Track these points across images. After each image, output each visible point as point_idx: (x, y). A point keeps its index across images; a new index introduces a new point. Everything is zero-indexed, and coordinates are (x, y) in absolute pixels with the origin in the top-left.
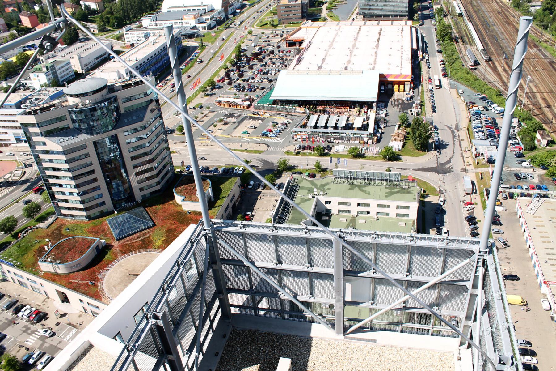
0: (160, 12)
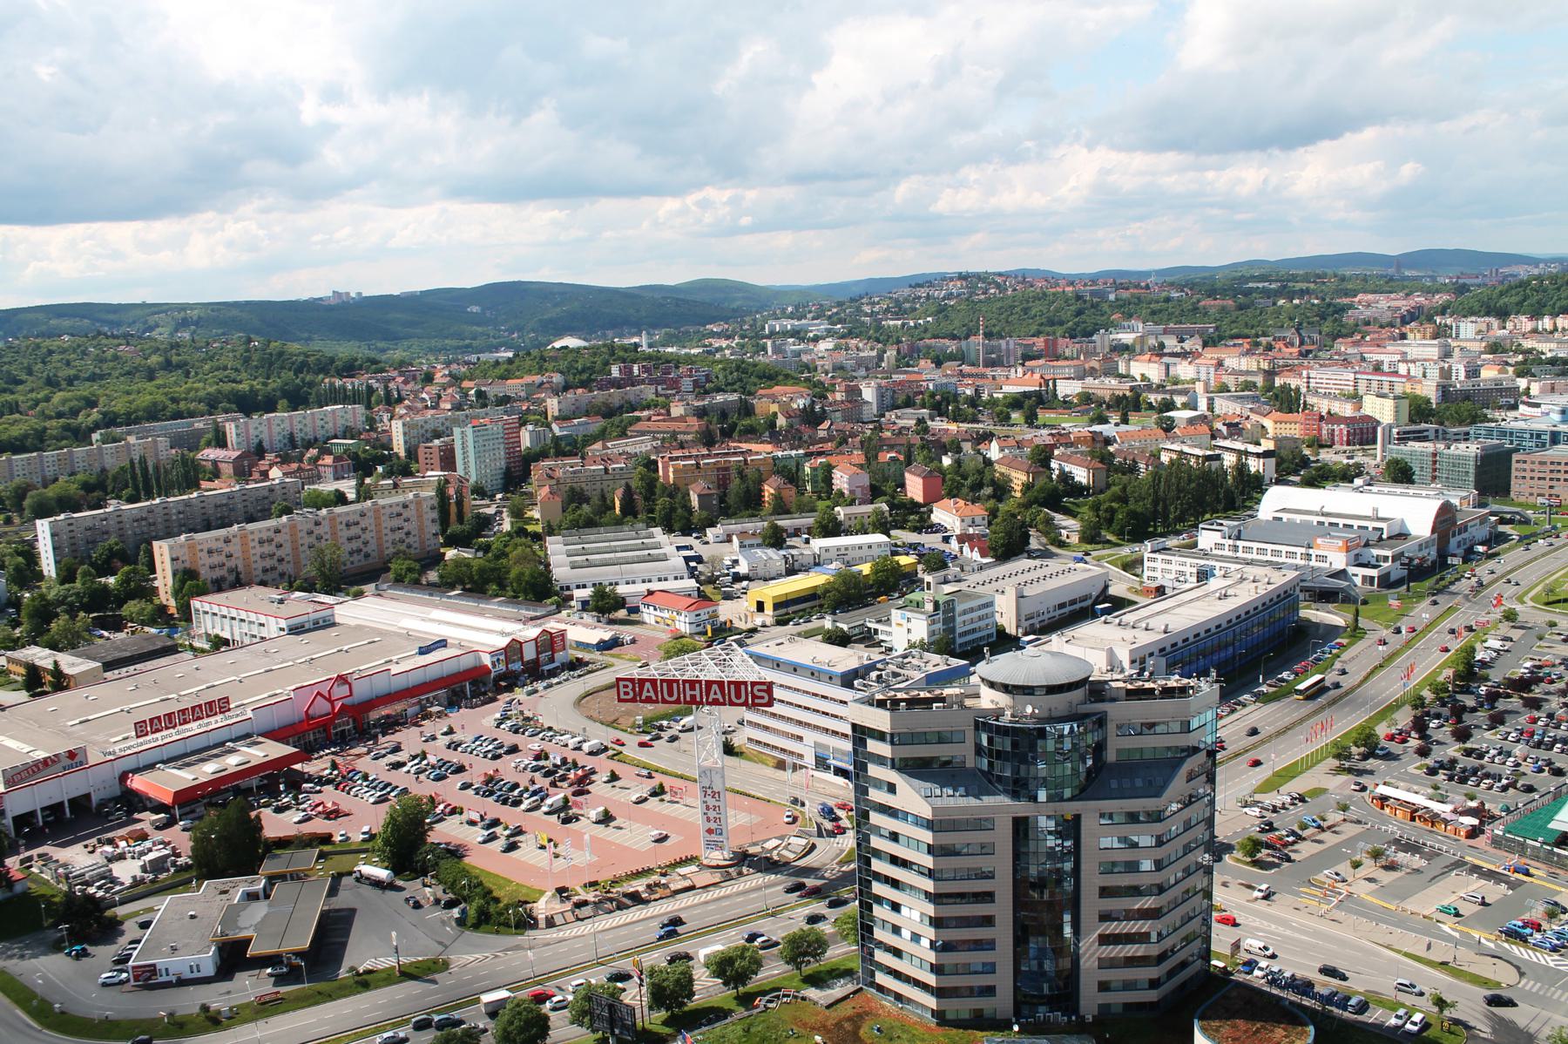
0: (1251, 516)
